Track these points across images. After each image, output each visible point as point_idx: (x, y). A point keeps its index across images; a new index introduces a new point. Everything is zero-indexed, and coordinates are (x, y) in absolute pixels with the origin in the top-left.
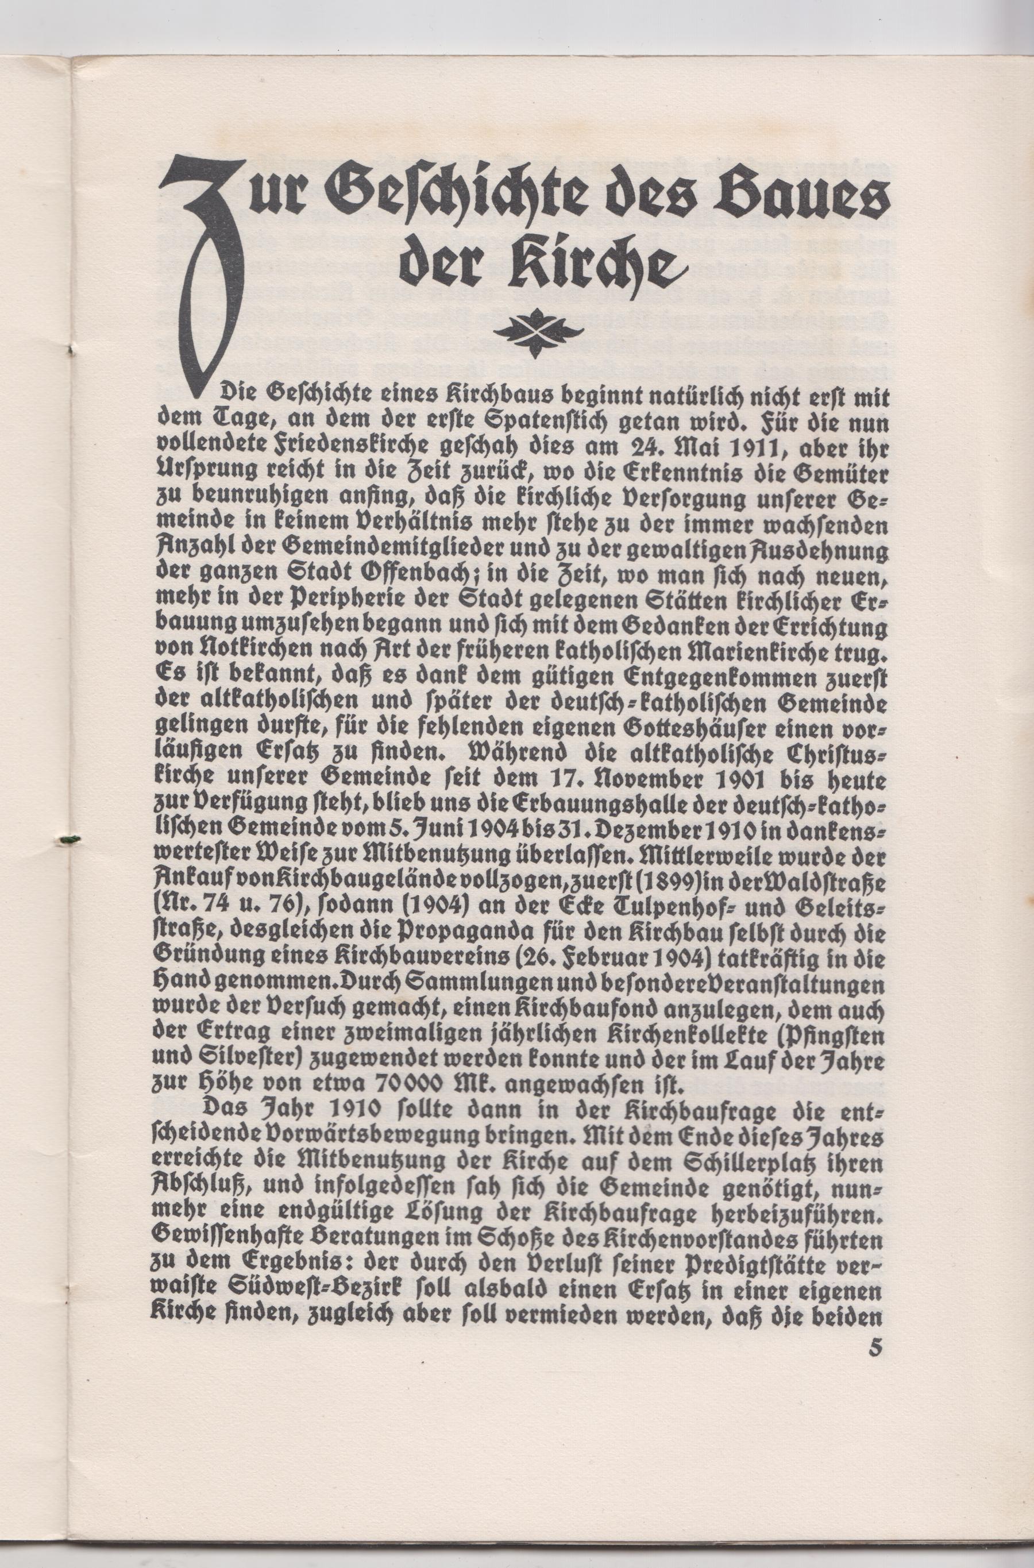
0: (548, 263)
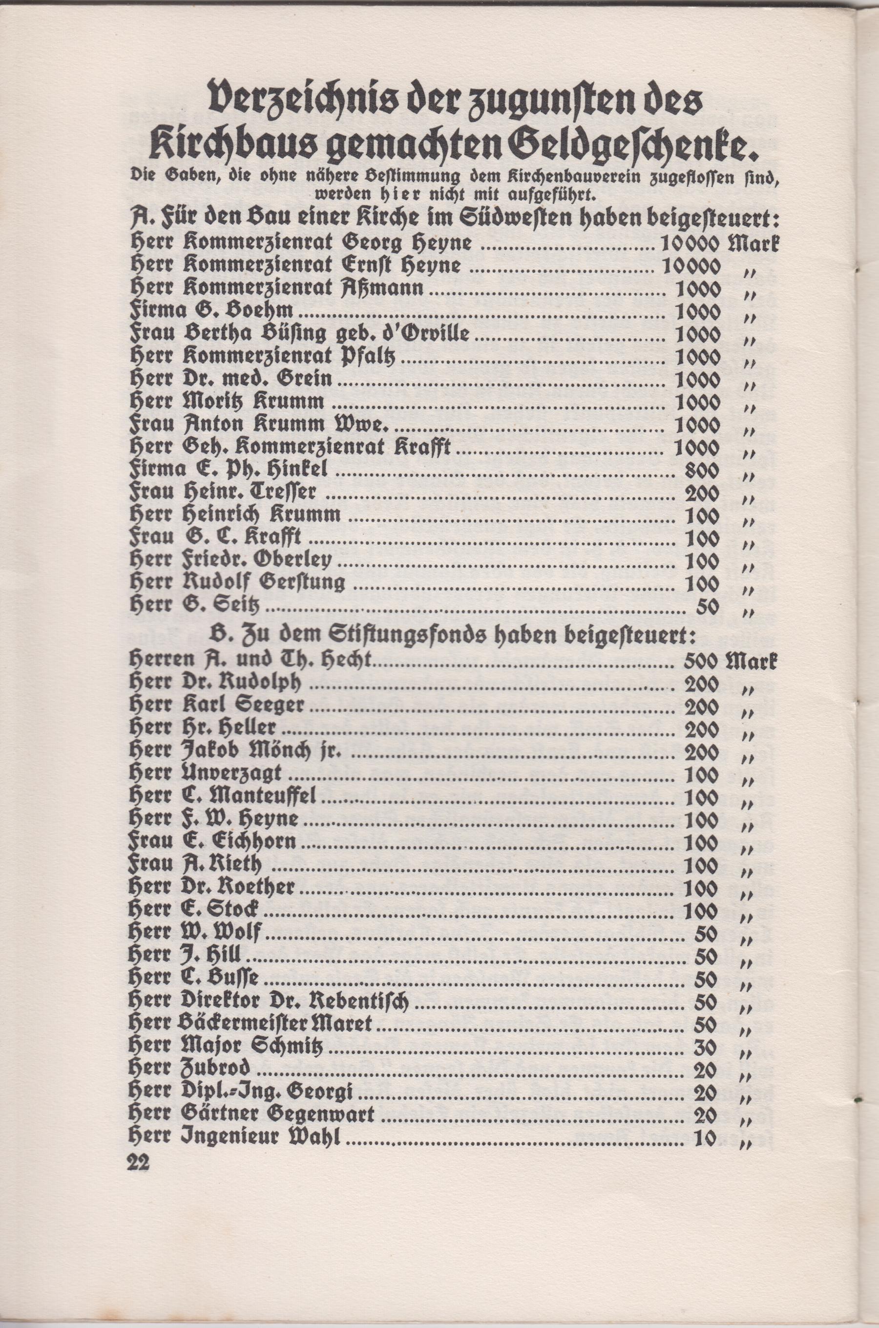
0: (173, 144)
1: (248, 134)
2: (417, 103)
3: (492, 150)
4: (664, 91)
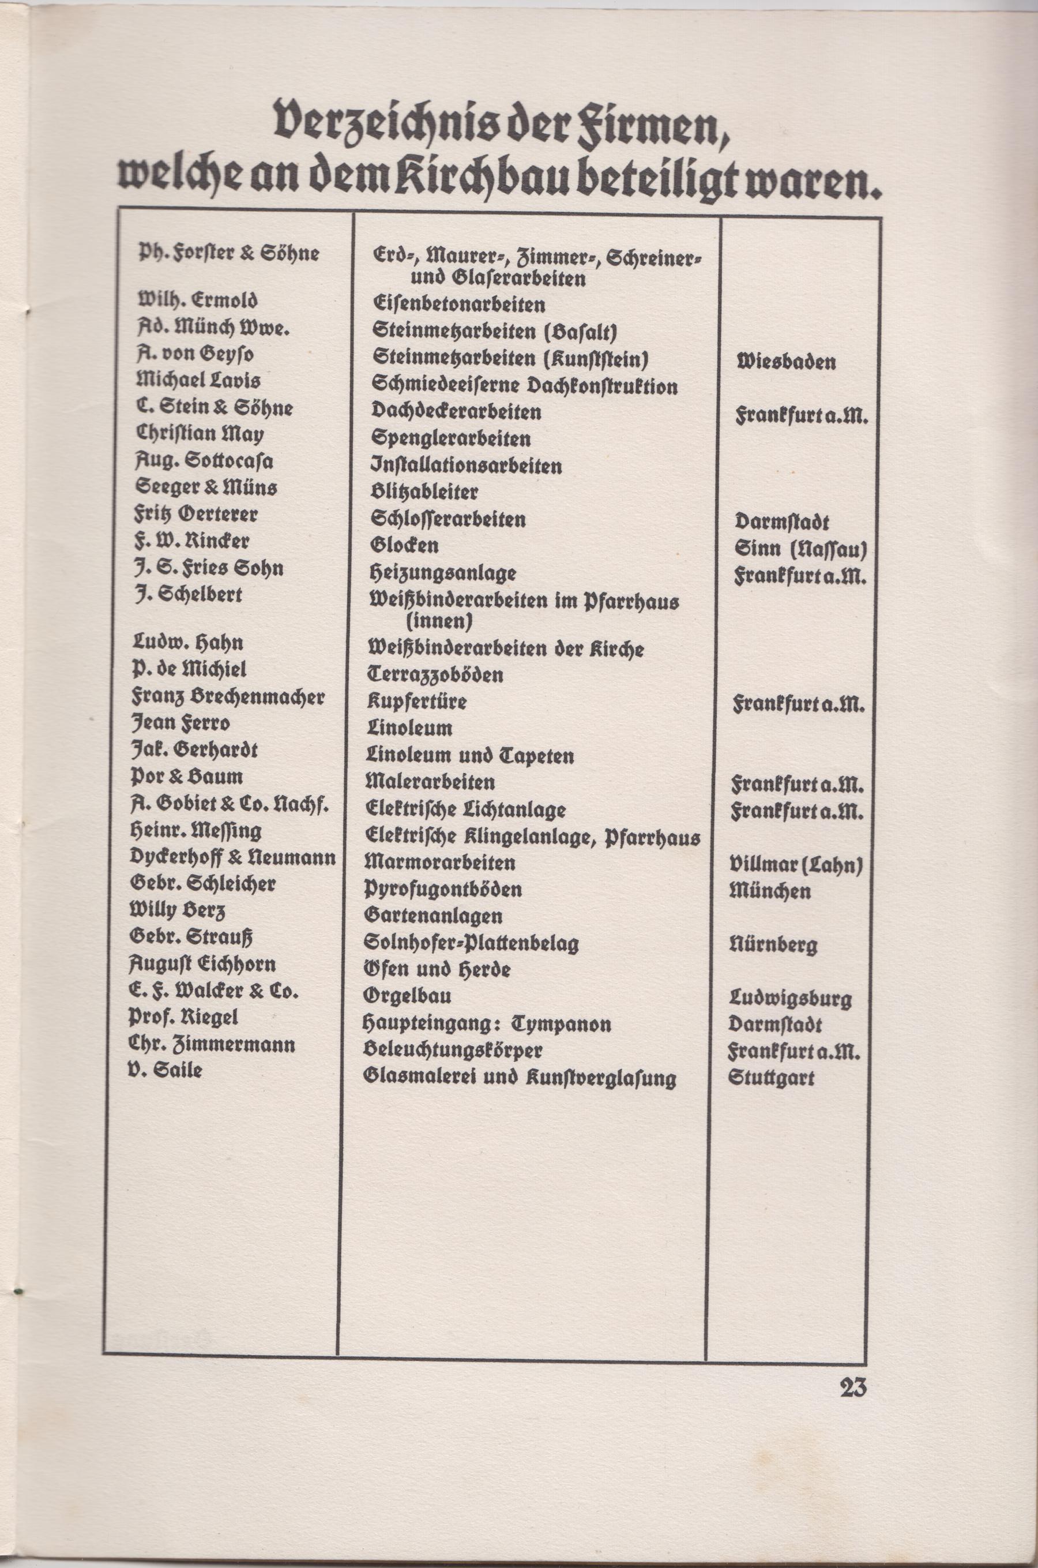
0: (424, 177)
1: (591, 168)
2: (519, 129)
3: (287, 180)
4: (531, 114)
